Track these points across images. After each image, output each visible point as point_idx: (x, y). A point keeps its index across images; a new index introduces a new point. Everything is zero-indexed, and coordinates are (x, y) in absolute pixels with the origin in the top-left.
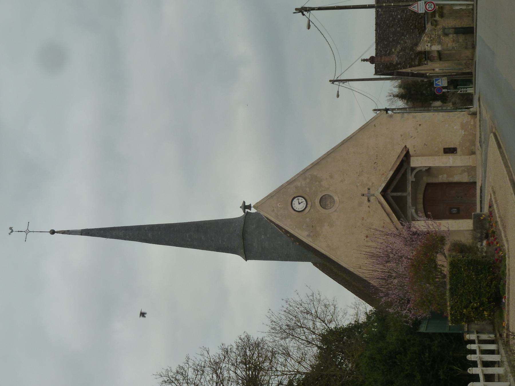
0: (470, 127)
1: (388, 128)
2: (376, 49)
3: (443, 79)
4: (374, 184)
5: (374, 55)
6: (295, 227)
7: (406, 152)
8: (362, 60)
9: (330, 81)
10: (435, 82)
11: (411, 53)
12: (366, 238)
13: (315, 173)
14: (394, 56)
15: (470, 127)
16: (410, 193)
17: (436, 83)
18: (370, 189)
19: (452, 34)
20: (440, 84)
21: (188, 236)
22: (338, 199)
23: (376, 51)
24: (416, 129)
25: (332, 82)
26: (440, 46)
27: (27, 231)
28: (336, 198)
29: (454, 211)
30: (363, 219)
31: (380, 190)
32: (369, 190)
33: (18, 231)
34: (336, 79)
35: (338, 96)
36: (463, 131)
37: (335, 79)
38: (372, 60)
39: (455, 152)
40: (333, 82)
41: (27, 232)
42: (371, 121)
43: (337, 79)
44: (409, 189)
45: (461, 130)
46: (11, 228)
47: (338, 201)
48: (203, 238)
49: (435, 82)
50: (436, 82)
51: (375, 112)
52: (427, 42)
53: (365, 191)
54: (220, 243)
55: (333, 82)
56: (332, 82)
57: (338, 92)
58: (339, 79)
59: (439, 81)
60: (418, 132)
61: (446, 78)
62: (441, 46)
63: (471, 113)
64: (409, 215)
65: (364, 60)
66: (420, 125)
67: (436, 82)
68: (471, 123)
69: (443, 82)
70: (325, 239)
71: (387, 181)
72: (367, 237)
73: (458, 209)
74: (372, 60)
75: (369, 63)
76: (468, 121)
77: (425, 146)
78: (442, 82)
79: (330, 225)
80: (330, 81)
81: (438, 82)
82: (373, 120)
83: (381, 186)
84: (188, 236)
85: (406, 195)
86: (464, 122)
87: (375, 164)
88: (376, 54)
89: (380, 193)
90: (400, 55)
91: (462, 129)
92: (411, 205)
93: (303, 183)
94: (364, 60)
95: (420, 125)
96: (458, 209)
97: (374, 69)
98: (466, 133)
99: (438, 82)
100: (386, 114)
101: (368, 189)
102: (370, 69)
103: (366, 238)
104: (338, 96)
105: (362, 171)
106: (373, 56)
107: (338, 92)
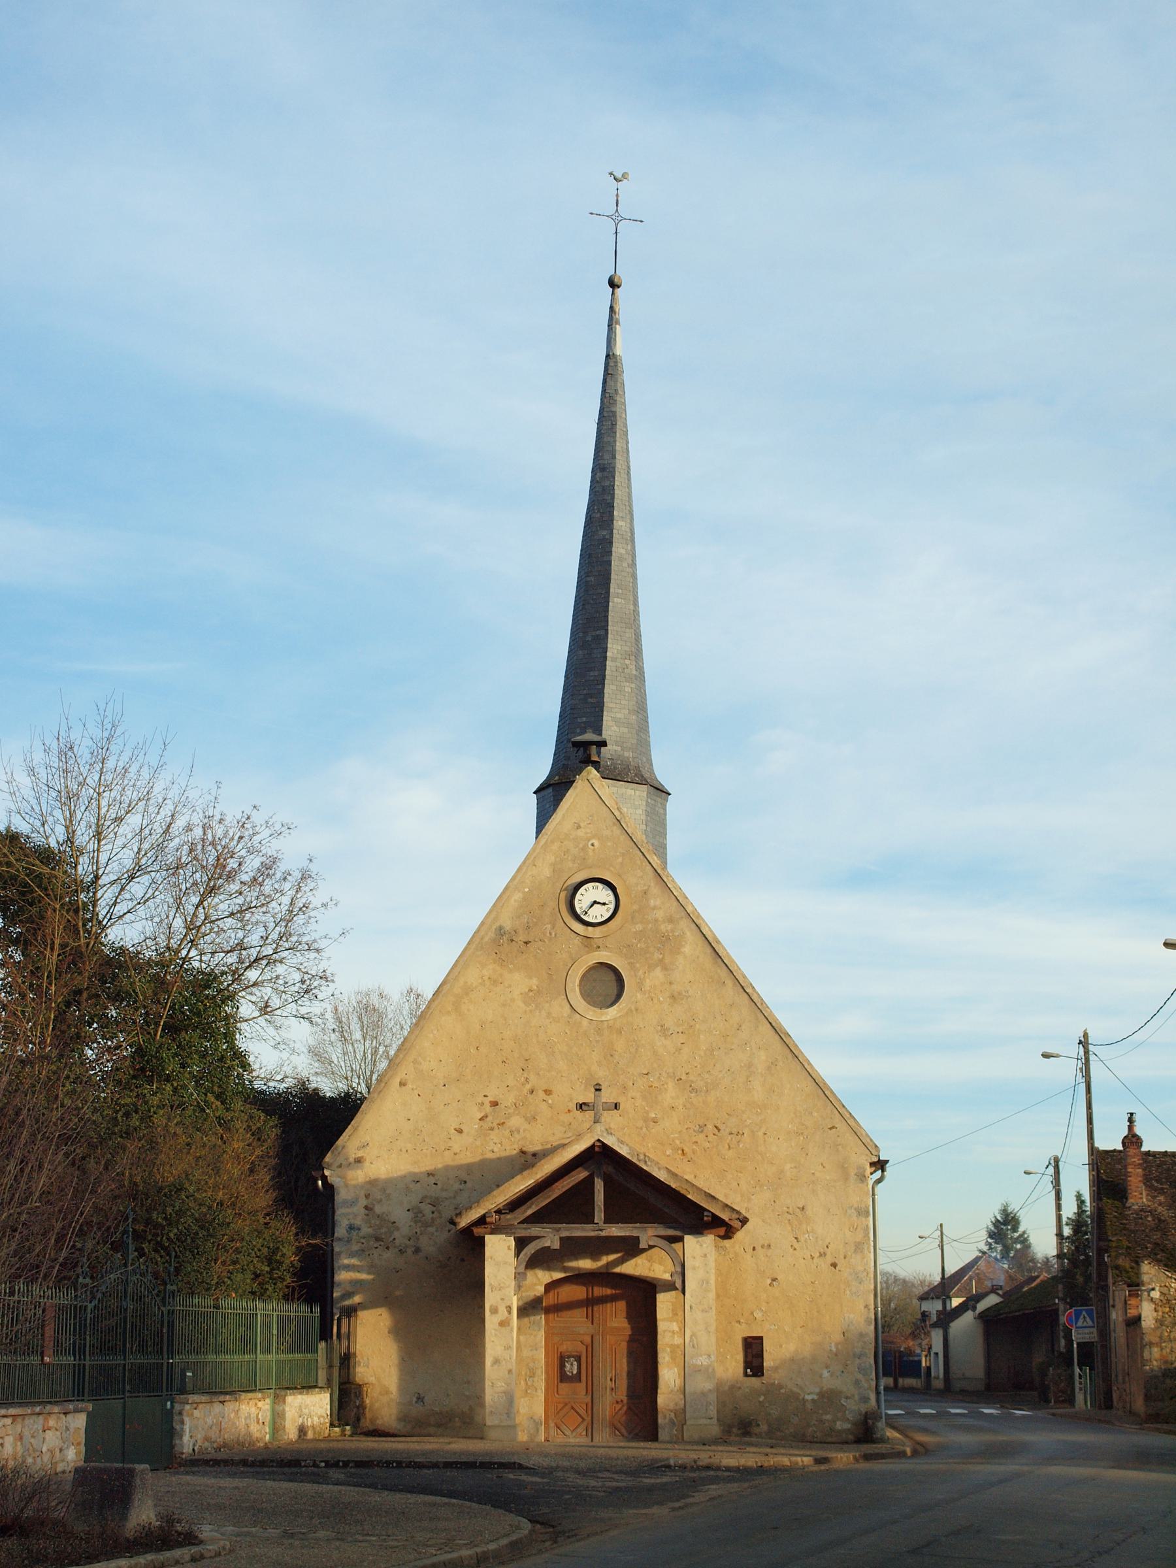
0: (828, 1417)
1: (824, 1167)
2: (1166, 1152)
3: (1092, 1330)
4: (652, 1123)
5: (1145, 1148)
6: (527, 890)
7: (727, 1220)
8: (1132, 1114)
9: (1086, 1035)
10: (1086, 1310)
11: (1149, 1245)
12: (490, 1102)
13: (687, 950)
14: (1145, 1200)
15: (828, 1417)
16: (603, 1234)
17: (1081, 1311)
18: (616, 1108)
19: (522, 1397)
20: (1080, 1324)
21: (598, 633)
22: (609, 1018)
23: (1160, 1153)
24: (822, 1255)
25: (1083, 1039)
26: (1153, 1326)
27: (620, 218)
28: (612, 1012)
29: (571, 1368)
30: (548, 1092)
31: (610, 1141)
32: (614, 1107)
33: (617, 195)
34: (1090, 1049)
35: (1046, 1056)
36: (816, 1397)
37: (1091, 1048)
38: (1132, 1140)
39: (749, 1370)
40: (1084, 1043)
41: (616, 218)
42: (848, 1116)
43: (1091, 1053)
44: (615, 1231)
45: (817, 1390)
46: (625, 176)
47: (603, 1019)
48: (592, 674)
49: (1086, 1310)
50: (1084, 1313)
51: (1052, 1162)
52: (1165, 1290)
53: (607, 1096)
54: (579, 720)
55: (1084, 1043)
56: (1083, 1039)
57: (1057, 1056)
58: (1092, 1058)
59: (1088, 1319)
60: (813, 1258)
61: (1096, 1339)
62: (1151, 1328)
63: (870, 1422)
64: (534, 1230)
65: (1131, 1120)
66: (834, 1265)
67: (1084, 1313)
68: (838, 1423)
69: (1087, 1330)
70: (489, 978)
71: (638, 1163)
72: (495, 1104)
73: (577, 1378)
74: (1132, 1140)
75: (1125, 1133)
76: (847, 1412)
77: (769, 1281)
78: (1085, 1327)
79: (531, 994)
80: (1086, 1035)
81: (1084, 1317)
82: (851, 1122)
83: (622, 1142)
84: (598, 633)
85: (596, 1221)
86: (843, 1402)
87: (715, 1129)
88: (1154, 1152)
89: (599, 1140)
90: (1146, 1217)
91: (821, 1395)
92: (565, 1234)
93: (660, 914)
94: (1131, 1120)
95: (834, 1265)
96: (577, 1378)
97: (1112, 1149)
98: (809, 1406)
99: (1084, 1317)
100: (870, 1161)
101: (616, 1104)
102: (1110, 1140)
103: (490, 1102)
104: (1046, 1056)
105: (694, 1090)
106: (1144, 1144)
107: (1057, 1056)
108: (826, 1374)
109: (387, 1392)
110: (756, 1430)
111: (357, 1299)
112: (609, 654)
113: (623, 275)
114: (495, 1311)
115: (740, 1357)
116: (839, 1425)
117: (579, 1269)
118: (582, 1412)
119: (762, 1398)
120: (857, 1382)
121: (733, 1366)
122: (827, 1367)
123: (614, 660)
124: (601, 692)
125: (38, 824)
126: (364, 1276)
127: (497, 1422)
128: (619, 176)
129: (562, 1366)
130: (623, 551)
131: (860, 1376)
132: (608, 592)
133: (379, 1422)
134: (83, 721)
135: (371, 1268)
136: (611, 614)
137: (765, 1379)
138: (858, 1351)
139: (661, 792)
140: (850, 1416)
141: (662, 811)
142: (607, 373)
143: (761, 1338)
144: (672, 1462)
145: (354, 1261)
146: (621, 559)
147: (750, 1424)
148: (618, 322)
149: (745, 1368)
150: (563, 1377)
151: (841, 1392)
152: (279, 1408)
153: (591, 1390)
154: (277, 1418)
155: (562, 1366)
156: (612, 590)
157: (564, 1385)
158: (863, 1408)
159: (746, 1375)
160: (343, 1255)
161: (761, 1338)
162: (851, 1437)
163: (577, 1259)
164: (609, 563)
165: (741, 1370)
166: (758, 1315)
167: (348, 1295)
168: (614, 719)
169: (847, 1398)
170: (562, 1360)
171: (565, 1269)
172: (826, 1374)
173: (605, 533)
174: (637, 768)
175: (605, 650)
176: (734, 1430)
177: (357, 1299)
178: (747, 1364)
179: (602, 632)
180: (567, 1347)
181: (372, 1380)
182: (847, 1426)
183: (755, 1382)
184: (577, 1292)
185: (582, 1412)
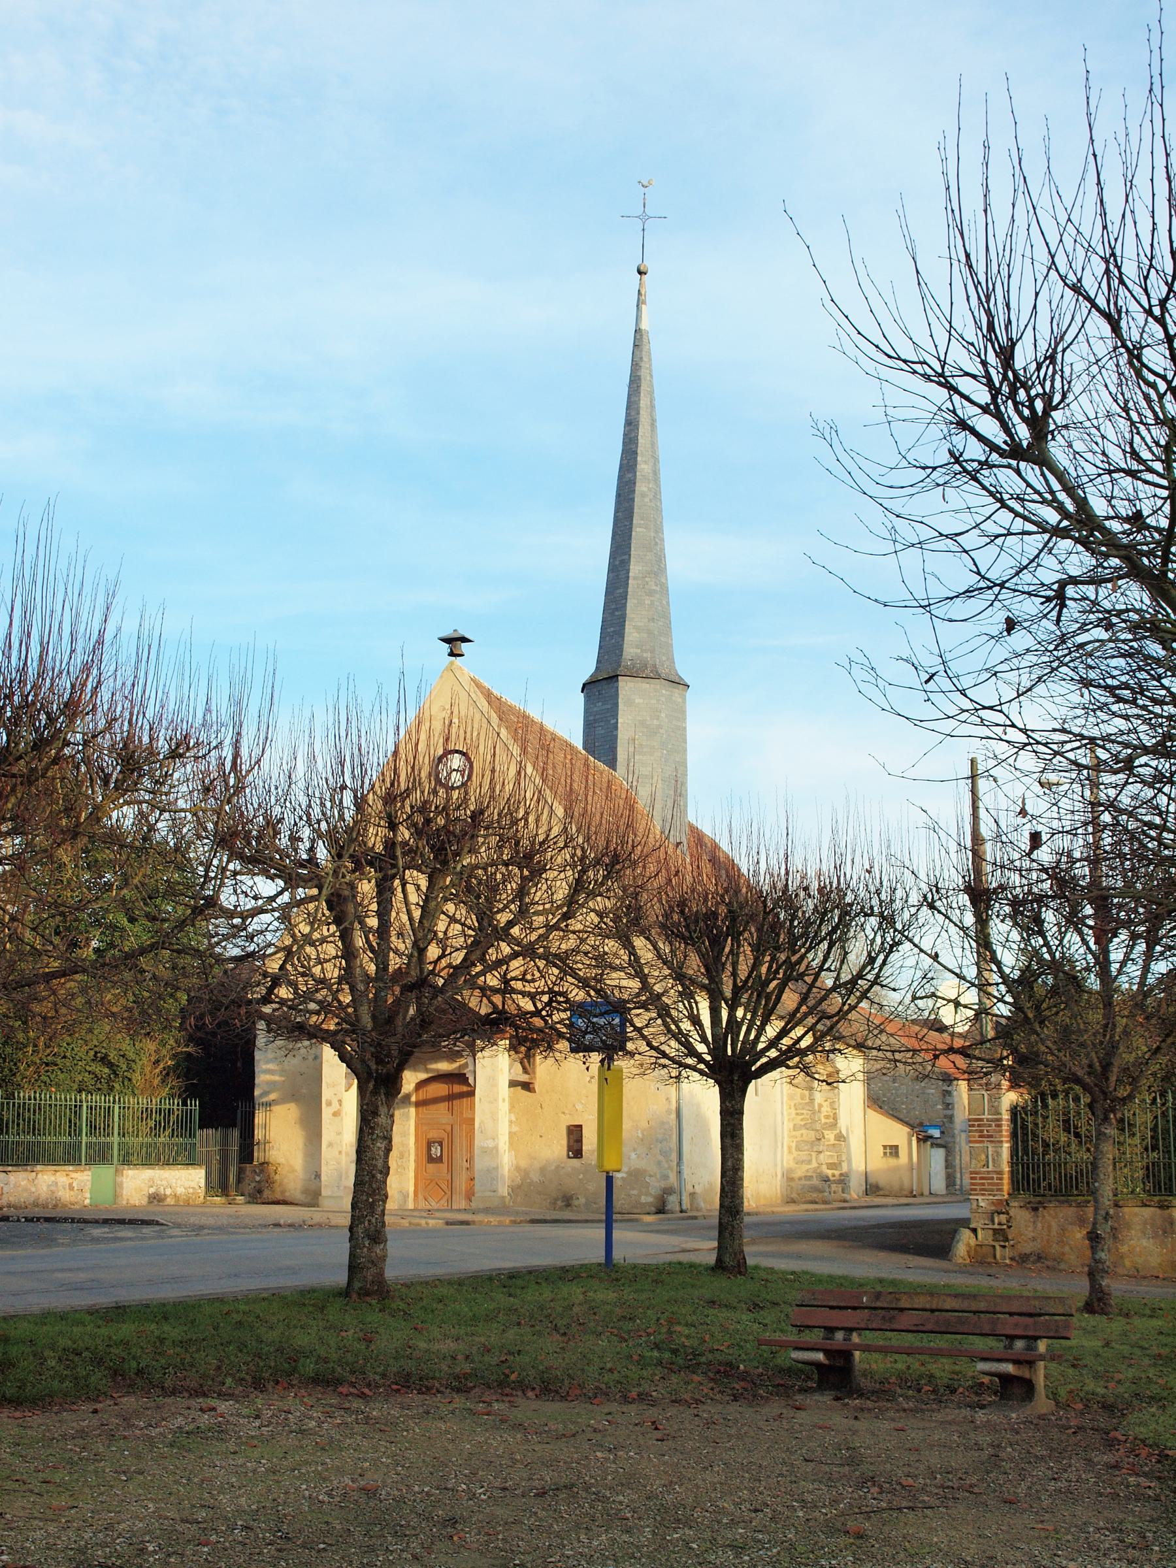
0: (635, 1192)
15: (635, 1192)
29: (436, 1151)
73: (439, 1160)
86: (647, 1179)
96: (439, 1160)
108: (633, 1156)
109: (293, 1170)
110: (576, 1202)
111: (272, 1096)
112: (631, 574)
113: (649, 264)
114: (329, 1104)
115: (564, 1142)
116: (643, 1199)
117: (438, 1070)
118: (444, 1187)
119: (581, 1176)
120: (659, 1163)
121: (558, 1147)
122: (634, 1150)
123: (635, 578)
124: (624, 606)
125: (214, 744)
126: (276, 1078)
127: (330, 1193)
128: (646, 183)
129: (429, 1149)
130: (645, 489)
131: (661, 1158)
132: (631, 524)
133: (287, 1194)
134: (978, 707)
135: (282, 1072)
136: (633, 542)
137: (583, 1161)
138: (660, 1137)
139: (679, 684)
140: (653, 1192)
141: (680, 700)
142: (636, 346)
143: (581, 1126)
144: (282, 1222)
145: (271, 1066)
146: (643, 495)
147: (571, 1197)
148: (644, 302)
149: (569, 1150)
150: (431, 1159)
151: (645, 1171)
152: (119, 1179)
153: (450, 1169)
154: (117, 1188)
155: (429, 1149)
156: (635, 522)
157: (431, 1165)
158: (663, 1184)
159: (569, 1157)
160: (261, 1063)
161: (581, 1126)
162: (653, 1209)
163: (436, 1062)
164: (633, 500)
165: (565, 1152)
166: (579, 1107)
167: (265, 1093)
168: (637, 628)
169: (650, 1176)
170: (429, 1145)
171: (427, 1071)
172: (633, 1156)
173: (630, 475)
174: (655, 666)
175: (628, 571)
176: (559, 1203)
177: (272, 1096)
178: (570, 1149)
179: (626, 557)
180: (433, 1134)
181: (282, 1161)
182: (650, 1199)
183: (575, 1162)
184: (441, 1089)
185: (444, 1187)
